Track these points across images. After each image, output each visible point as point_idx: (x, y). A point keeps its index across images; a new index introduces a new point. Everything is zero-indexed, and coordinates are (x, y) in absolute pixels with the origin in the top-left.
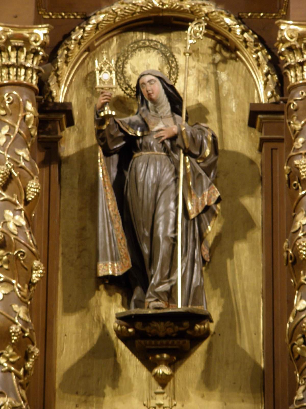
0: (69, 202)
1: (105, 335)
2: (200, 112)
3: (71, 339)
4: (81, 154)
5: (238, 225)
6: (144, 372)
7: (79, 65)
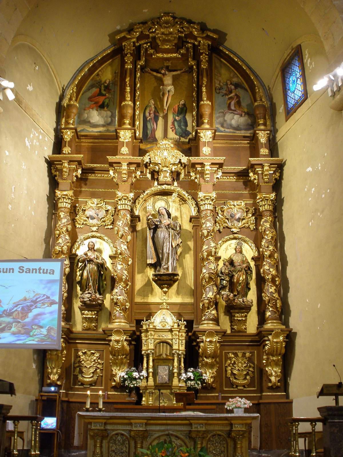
0: (139, 243)
1: (149, 280)
2: (176, 218)
3: (140, 281)
4: (142, 229)
5: (187, 249)
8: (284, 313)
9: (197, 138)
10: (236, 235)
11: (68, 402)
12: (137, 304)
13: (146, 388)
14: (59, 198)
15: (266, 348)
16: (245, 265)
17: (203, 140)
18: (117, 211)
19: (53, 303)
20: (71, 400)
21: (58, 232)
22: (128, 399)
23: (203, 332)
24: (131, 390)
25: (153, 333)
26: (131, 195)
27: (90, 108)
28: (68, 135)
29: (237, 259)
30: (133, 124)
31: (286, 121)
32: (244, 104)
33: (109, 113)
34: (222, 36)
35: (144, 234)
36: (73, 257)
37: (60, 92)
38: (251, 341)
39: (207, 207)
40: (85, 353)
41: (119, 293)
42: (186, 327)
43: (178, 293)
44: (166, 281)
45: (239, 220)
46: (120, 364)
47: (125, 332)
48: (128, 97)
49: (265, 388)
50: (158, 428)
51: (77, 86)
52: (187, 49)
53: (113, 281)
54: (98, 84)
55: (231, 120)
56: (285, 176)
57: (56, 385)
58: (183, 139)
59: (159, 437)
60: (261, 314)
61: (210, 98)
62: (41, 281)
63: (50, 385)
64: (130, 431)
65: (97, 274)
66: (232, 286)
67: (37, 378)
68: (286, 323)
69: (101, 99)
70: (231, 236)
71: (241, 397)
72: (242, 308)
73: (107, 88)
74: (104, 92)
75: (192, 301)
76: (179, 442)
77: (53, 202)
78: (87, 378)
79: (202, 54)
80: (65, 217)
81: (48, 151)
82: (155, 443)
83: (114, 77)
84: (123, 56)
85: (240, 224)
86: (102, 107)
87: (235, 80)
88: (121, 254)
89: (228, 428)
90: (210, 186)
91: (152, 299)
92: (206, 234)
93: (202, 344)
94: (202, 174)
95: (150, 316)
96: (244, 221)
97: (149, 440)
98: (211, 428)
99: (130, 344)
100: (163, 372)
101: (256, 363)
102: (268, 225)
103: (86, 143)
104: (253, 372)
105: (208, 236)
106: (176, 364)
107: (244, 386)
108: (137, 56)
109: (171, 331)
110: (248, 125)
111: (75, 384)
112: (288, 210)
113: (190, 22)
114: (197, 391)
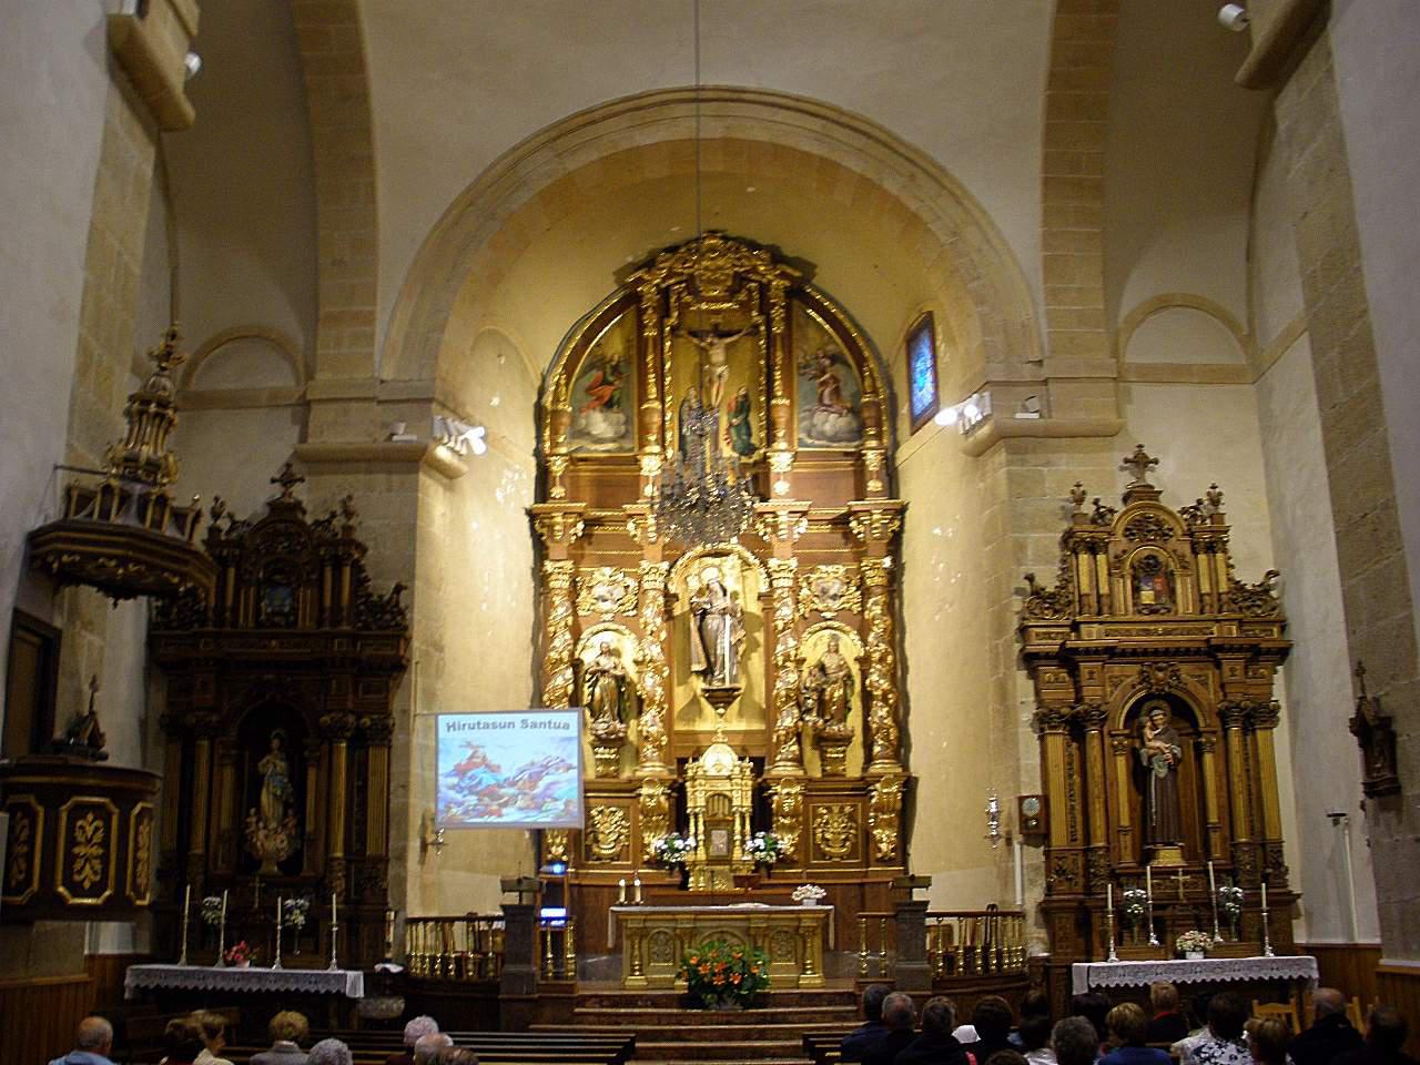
0: (679, 637)
1: (695, 696)
2: (735, 595)
3: (681, 697)
4: (683, 614)
5: (754, 645)
6: (713, 711)
7: (126, 859)
8: (901, 748)
9: (765, 461)
10: (829, 623)
11: (580, 886)
12: (678, 733)
13: (694, 864)
14: (551, 574)
15: (874, 801)
16: (842, 674)
17: (774, 470)
18: (641, 592)
19: (570, 768)
20: (584, 883)
21: (552, 629)
22: (668, 880)
23: (778, 780)
24: (672, 866)
25: (703, 782)
26: (665, 566)
27: (588, 408)
28: (558, 466)
29: (831, 662)
30: (662, 442)
31: (912, 434)
32: (846, 393)
33: (622, 417)
34: (808, 269)
35: (687, 625)
36: (576, 664)
37: (537, 383)
38: (852, 790)
39: (784, 582)
40: (601, 812)
41: (650, 721)
42: (752, 771)
43: (741, 714)
44: (721, 698)
45: (834, 597)
46: (656, 828)
47: (662, 782)
48: (653, 391)
49: (872, 859)
50: (708, 924)
51: (565, 367)
52: (750, 291)
53: (640, 705)
54: (598, 362)
55: (824, 423)
56: (907, 527)
57: (562, 863)
58: (744, 460)
59: (710, 935)
60: (868, 745)
61: (788, 393)
62: (552, 739)
63: (552, 862)
64: (675, 928)
65: (616, 692)
66: (822, 706)
67: (532, 853)
68: (905, 767)
69: (607, 391)
70: (823, 624)
71: (813, 885)
72: (839, 740)
73: (615, 369)
74: (611, 379)
75: (763, 727)
76: (735, 941)
77: (541, 579)
78: (606, 849)
79: (774, 305)
80: (561, 604)
81: (528, 498)
82: (705, 942)
83: (628, 349)
84: (641, 313)
85: (836, 605)
86: (609, 405)
87: (831, 348)
88: (650, 661)
89: (796, 924)
90: (788, 550)
91: (700, 726)
92: (780, 628)
93: (775, 798)
94: (775, 527)
95: (697, 755)
96: (843, 599)
97: (699, 939)
98: (775, 923)
99: (669, 796)
100: (719, 838)
101: (860, 821)
102: (877, 610)
103: (586, 472)
104: (856, 836)
105: (784, 630)
106: (738, 827)
107: (842, 858)
108: (664, 311)
109: (729, 778)
110: (850, 432)
111: (588, 859)
112: (911, 584)
113: (753, 246)
114: (769, 866)
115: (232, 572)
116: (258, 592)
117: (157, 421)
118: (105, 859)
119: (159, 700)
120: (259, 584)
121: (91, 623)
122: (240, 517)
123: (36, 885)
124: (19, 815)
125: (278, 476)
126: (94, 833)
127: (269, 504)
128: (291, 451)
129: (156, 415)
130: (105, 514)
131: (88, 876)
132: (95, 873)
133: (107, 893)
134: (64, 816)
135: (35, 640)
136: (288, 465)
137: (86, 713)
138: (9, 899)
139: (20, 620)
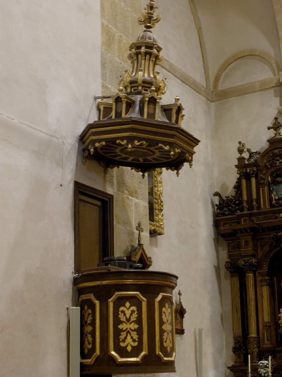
115: (253, 180)
116: (269, 190)
117: (148, 56)
118: (139, 331)
119: (224, 254)
120: (269, 184)
121: (136, 192)
122: (253, 150)
123: (98, 352)
124: (86, 307)
125: (271, 125)
126: (131, 315)
127: (268, 141)
128: (277, 111)
129: (146, 53)
130: (118, 114)
131: (129, 343)
132: (134, 341)
133: (143, 353)
134: (111, 305)
135: (99, 203)
136: (276, 119)
137: (136, 246)
138: (85, 361)
139: (81, 191)
